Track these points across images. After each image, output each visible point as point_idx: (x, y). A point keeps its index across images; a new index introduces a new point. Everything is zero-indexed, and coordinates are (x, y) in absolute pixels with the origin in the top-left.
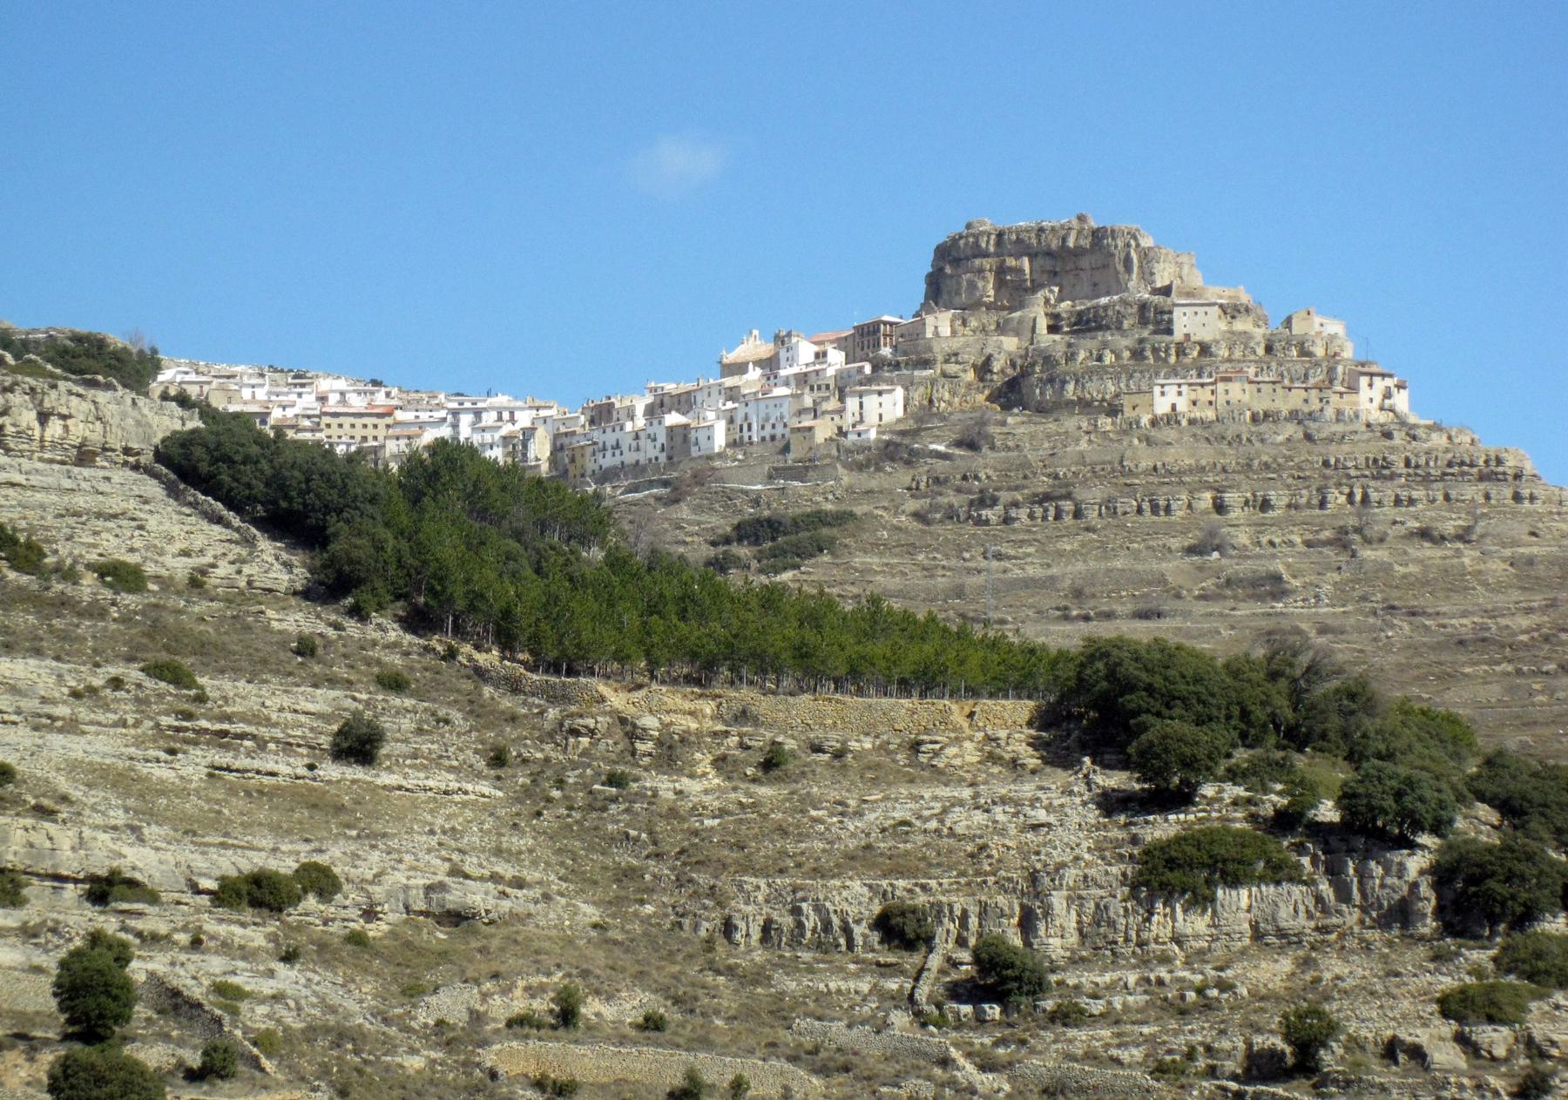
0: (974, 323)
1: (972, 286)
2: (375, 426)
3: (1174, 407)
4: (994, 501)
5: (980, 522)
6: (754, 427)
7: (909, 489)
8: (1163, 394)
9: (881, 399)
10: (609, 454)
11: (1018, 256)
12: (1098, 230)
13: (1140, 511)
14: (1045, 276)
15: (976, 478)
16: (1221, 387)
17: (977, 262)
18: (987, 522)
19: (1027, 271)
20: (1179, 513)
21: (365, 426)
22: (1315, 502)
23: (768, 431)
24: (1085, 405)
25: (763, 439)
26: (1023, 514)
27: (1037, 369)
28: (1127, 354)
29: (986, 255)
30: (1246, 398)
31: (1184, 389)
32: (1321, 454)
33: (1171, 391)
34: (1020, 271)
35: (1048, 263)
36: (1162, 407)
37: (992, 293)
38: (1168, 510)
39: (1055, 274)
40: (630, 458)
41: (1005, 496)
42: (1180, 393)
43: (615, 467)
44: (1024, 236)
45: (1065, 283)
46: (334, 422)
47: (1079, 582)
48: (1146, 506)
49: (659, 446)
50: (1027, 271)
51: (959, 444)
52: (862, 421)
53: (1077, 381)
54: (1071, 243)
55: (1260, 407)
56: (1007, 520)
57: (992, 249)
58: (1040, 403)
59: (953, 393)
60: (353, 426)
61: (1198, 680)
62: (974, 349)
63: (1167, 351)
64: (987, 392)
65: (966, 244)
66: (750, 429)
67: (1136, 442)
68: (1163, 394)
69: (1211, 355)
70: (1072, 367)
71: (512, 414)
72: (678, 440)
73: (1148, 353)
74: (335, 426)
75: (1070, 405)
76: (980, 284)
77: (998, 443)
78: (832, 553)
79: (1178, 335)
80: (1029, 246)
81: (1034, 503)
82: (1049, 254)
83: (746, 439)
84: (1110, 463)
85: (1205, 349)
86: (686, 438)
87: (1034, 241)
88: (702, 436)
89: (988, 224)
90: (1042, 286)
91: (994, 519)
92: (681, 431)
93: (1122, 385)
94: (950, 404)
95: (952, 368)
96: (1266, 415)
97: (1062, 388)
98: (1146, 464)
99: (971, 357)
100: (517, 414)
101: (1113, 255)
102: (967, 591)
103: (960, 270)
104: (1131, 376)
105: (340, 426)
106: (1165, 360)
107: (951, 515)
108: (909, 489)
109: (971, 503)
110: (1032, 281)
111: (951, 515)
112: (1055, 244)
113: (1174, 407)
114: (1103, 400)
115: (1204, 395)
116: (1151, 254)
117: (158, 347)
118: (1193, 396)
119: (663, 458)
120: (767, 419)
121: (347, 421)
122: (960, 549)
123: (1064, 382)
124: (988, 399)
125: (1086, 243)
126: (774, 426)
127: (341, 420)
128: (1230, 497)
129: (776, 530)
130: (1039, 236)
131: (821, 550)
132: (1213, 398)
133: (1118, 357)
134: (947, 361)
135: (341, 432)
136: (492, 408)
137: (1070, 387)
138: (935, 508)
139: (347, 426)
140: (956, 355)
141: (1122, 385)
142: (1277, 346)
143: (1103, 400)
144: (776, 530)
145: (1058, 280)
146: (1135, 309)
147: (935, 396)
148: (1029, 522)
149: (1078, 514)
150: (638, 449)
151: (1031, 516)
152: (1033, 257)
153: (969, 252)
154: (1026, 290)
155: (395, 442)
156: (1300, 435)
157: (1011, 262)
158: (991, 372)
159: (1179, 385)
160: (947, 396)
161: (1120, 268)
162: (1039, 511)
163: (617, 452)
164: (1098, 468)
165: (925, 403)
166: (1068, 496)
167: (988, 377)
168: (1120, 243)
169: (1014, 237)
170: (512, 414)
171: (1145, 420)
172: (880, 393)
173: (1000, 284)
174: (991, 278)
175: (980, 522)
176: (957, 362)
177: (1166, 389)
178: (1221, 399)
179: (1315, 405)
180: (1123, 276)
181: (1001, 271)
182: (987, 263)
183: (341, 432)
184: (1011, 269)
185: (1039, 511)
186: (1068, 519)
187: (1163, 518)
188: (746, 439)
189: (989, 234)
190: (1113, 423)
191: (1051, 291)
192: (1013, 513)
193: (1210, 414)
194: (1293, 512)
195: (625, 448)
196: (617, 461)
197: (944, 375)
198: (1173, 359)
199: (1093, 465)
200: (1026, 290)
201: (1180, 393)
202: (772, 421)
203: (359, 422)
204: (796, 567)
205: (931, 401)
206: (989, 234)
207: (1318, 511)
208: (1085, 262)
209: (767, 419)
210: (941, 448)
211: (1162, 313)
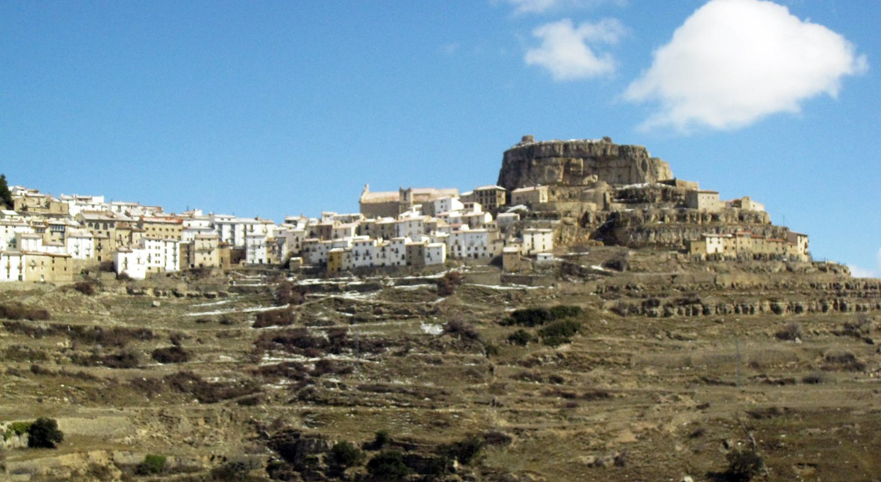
0: (558, 193)
1: (551, 173)
2: (173, 230)
3: (716, 250)
4: (657, 304)
5: (652, 315)
6: (464, 248)
10: (361, 258)
11: (578, 158)
13: (737, 311)
14: (590, 170)
15: (635, 288)
16: (738, 239)
17: (554, 160)
18: (655, 316)
19: (582, 165)
20: (757, 312)
21: (167, 230)
22: (820, 308)
23: (472, 251)
24: (660, 246)
25: (469, 255)
26: (675, 311)
28: (675, 218)
29: (557, 156)
30: (750, 246)
31: (721, 240)
32: (808, 281)
33: (715, 240)
34: (578, 166)
35: (593, 163)
36: (711, 250)
37: (561, 177)
38: (752, 311)
40: (377, 261)
41: (663, 301)
43: (366, 267)
44: (581, 147)
46: (150, 226)
47: (753, 358)
48: (740, 308)
50: (582, 165)
52: (533, 248)
53: (656, 232)
54: (609, 153)
55: (757, 251)
56: (667, 314)
57: (562, 153)
58: (632, 243)
59: (572, 234)
60: (161, 230)
61: (39, 293)
62: (578, 209)
63: (697, 218)
65: (546, 149)
66: (459, 248)
71: (252, 226)
72: (415, 253)
74: (150, 229)
76: (557, 172)
77: (632, 267)
78: (581, 333)
79: (701, 209)
80: (584, 153)
81: (680, 305)
82: (595, 158)
85: (715, 217)
87: (587, 150)
88: (433, 254)
89: (544, 142)
91: (659, 313)
93: (680, 235)
96: (760, 255)
98: (728, 284)
99: (576, 213)
100: (255, 227)
103: (542, 164)
105: (154, 229)
106: (696, 223)
107: (633, 310)
109: (643, 304)
111: (633, 310)
112: (599, 153)
113: (716, 250)
114: (671, 243)
115: (730, 243)
116: (656, 162)
117: (6, 175)
118: (725, 244)
119: (403, 263)
120: (472, 244)
121: (157, 227)
122: (653, 333)
123: (649, 233)
124: (590, 238)
126: (476, 249)
127: (155, 226)
128: (781, 304)
131: (575, 331)
132: (734, 245)
134: (566, 216)
135: (154, 233)
136: (241, 223)
137: (653, 235)
138: (623, 306)
139: (157, 230)
142: (745, 217)
146: (660, 192)
147: (563, 235)
148: (678, 316)
149: (706, 312)
150: (384, 256)
151: (680, 312)
152: (585, 159)
153: (547, 154)
154: (579, 176)
155: (200, 241)
156: (784, 268)
157: (574, 161)
160: (569, 236)
161: (640, 168)
162: (683, 309)
163: (367, 258)
164: (704, 285)
166: (698, 301)
168: (638, 154)
169: (575, 147)
170: (252, 226)
171: (703, 257)
172: (543, 233)
173: (566, 172)
174: (562, 168)
175: (652, 315)
176: (571, 217)
177: (713, 239)
178: (739, 246)
179: (781, 251)
181: (568, 165)
182: (560, 160)
183: (154, 233)
186: (700, 314)
187: (749, 315)
191: (594, 178)
192: (670, 310)
193: (733, 255)
194: (811, 314)
195: (374, 256)
196: (367, 262)
197: (566, 223)
198: (700, 222)
199: (700, 283)
200: (579, 176)
202: (476, 245)
203: (164, 227)
204: (567, 342)
205: (561, 238)
207: (823, 314)
208: (613, 164)
209: (472, 244)
210: (600, 268)
211: (676, 195)
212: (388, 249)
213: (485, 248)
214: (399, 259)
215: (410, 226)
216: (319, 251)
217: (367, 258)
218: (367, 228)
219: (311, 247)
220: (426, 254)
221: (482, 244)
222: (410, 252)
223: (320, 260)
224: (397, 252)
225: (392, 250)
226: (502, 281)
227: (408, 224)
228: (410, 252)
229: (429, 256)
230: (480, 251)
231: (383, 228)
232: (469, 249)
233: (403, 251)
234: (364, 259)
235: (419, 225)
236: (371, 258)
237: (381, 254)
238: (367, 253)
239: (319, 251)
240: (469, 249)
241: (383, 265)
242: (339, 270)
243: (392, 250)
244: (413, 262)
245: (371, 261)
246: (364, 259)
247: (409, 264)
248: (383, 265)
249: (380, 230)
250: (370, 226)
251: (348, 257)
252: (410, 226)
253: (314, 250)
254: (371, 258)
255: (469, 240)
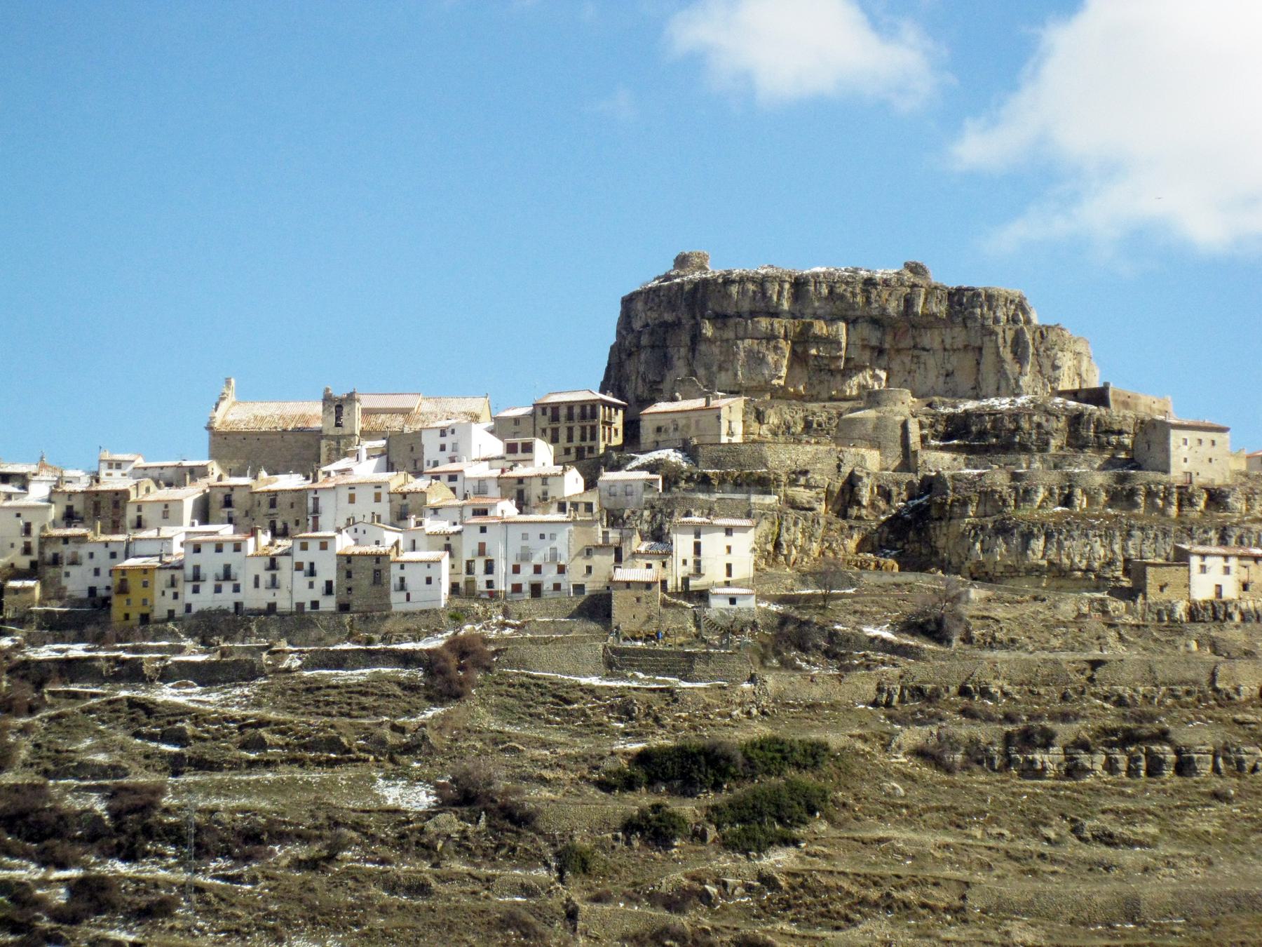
1: (756, 360)
4: (1047, 740)
6: (501, 567)
7: (875, 704)
8: (1203, 569)
9: (729, 541)
10: (207, 588)
11: (831, 320)
12: (960, 291)
14: (867, 355)
25: (517, 588)
27: (971, 510)
28: (1103, 497)
31: (1233, 562)
35: (874, 337)
36: (1202, 591)
37: (784, 372)
39: (880, 351)
40: (255, 599)
41: (1065, 732)
42: (1227, 570)
44: (840, 289)
45: (896, 366)
49: (320, 582)
51: (911, 626)
52: (698, 572)
53: (1049, 536)
56: (1073, 770)
57: (786, 305)
58: (980, 565)
64: (857, 537)
66: (489, 568)
67: (1194, 646)
68: (1203, 569)
69: (1226, 508)
70: (1025, 512)
72: (363, 580)
73: (1140, 500)
75: (1035, 571)
76: (771, 358)
79: (1176, 474)
82: (877, 322)
83: (481, 586)
84: (1195, 683)
85: (1216, 498)
86: (378, 578)
87: (859, 299)
90: (860, 368)
92: (372, 564)
93: (1117, 548)
94: (804, 551)
95: (802, 495)
97: (1026, 546)
99: (824, 476)
101: (993, 333)
102: (1144, 908)
104: (1129, 535)
106: (1163, 512)
107: (977, 756)
108: (875, 704)
110: (848, 360)
111: (977, 756)
114: (1089, 569)
116: (1052, 337)
119: (329, 604)
120: (526, 556)
123: (1027, 537)
124: (860, 548)
125: (940, 309)
126: (538, 569)
129: (724, 773)
130: (867, 293)
131: (811, 811)
133: (1092, 499)
134: (793, 483)
137: (1038, 544)
140: (805, 473)
141: (1117, 548)
143: (1089, 569)
144: (724, 773)
145: (883, 363)
146: (1062, 424)
147: (785, 537)
148: (1107, 777)
150: (274, 584)
151: (1111, 766)
152: (851, 322)
153: (746, 306)
157: (820, 328)
158: (859, 504)
159: (1226, 557)
161: (1007, 354)
163: (227, 587)
164: (1180, 690)
165: (770, 547)
166: (1163, 736)
167: (854, 511)
171: (1181, 610)
172: (729, 531)
173: (798, 358)
174: (786, 347)
176: (808, 486)
177: (1209, 561)
180: (1011, 367)
181: (802, 340)
182: (780, 325)
184: (818, 340)
185: (1122, 760)
188: (481, 586)
189: (781, 282)
190: (1129, 611)
191: (876, 377)
192: (1083, 758)
195: (246, 582)
196: (227, 599)
197: (793, 504)
198: (1173, 511)
199: (1170, 683)
200: (832, 372)
201: (1227, 570)
202: (536, 560)
205: (777, 545)
206: (781, 282)
208: (931, 339)
209: (526, 556)
212: (285, 563)
213: (561, 570)
214: (317, 593)
215: (352, 499)
216: (88, 565)
217: (227, 587)
218: (228, 503)
219: (66, 551)
220: (395, 581)
221: (554, 556)
222: (349, 575)
223: (92, 591)
224: (312, 573)
225: (299, 567)
226: (610, 664)
227: (345, 493)
228: (349, 575)
229: (402, 586)
230: (549, 577)
231: (273, 504)
232: (516, 570)
233: (328, 571)
234: (218, 590)
235: (378, 498)
236: (237, 589)
237: (265, 577)
238: (227, 575)
239: (88, 565)
240: (516, 570)
241: (272, 607)
242: (145, 619)
243: (299, 567)
244: (356, 603)
245: (238, 597)
246: (218, 590)
247: (344, 608)
248: (272, 607)
249: (265, 508)
250: (236, 497)
251: (173, 584)
252: (352, 499)
253: (75, 562)
254: (237, 589)
255: (516, 545)
